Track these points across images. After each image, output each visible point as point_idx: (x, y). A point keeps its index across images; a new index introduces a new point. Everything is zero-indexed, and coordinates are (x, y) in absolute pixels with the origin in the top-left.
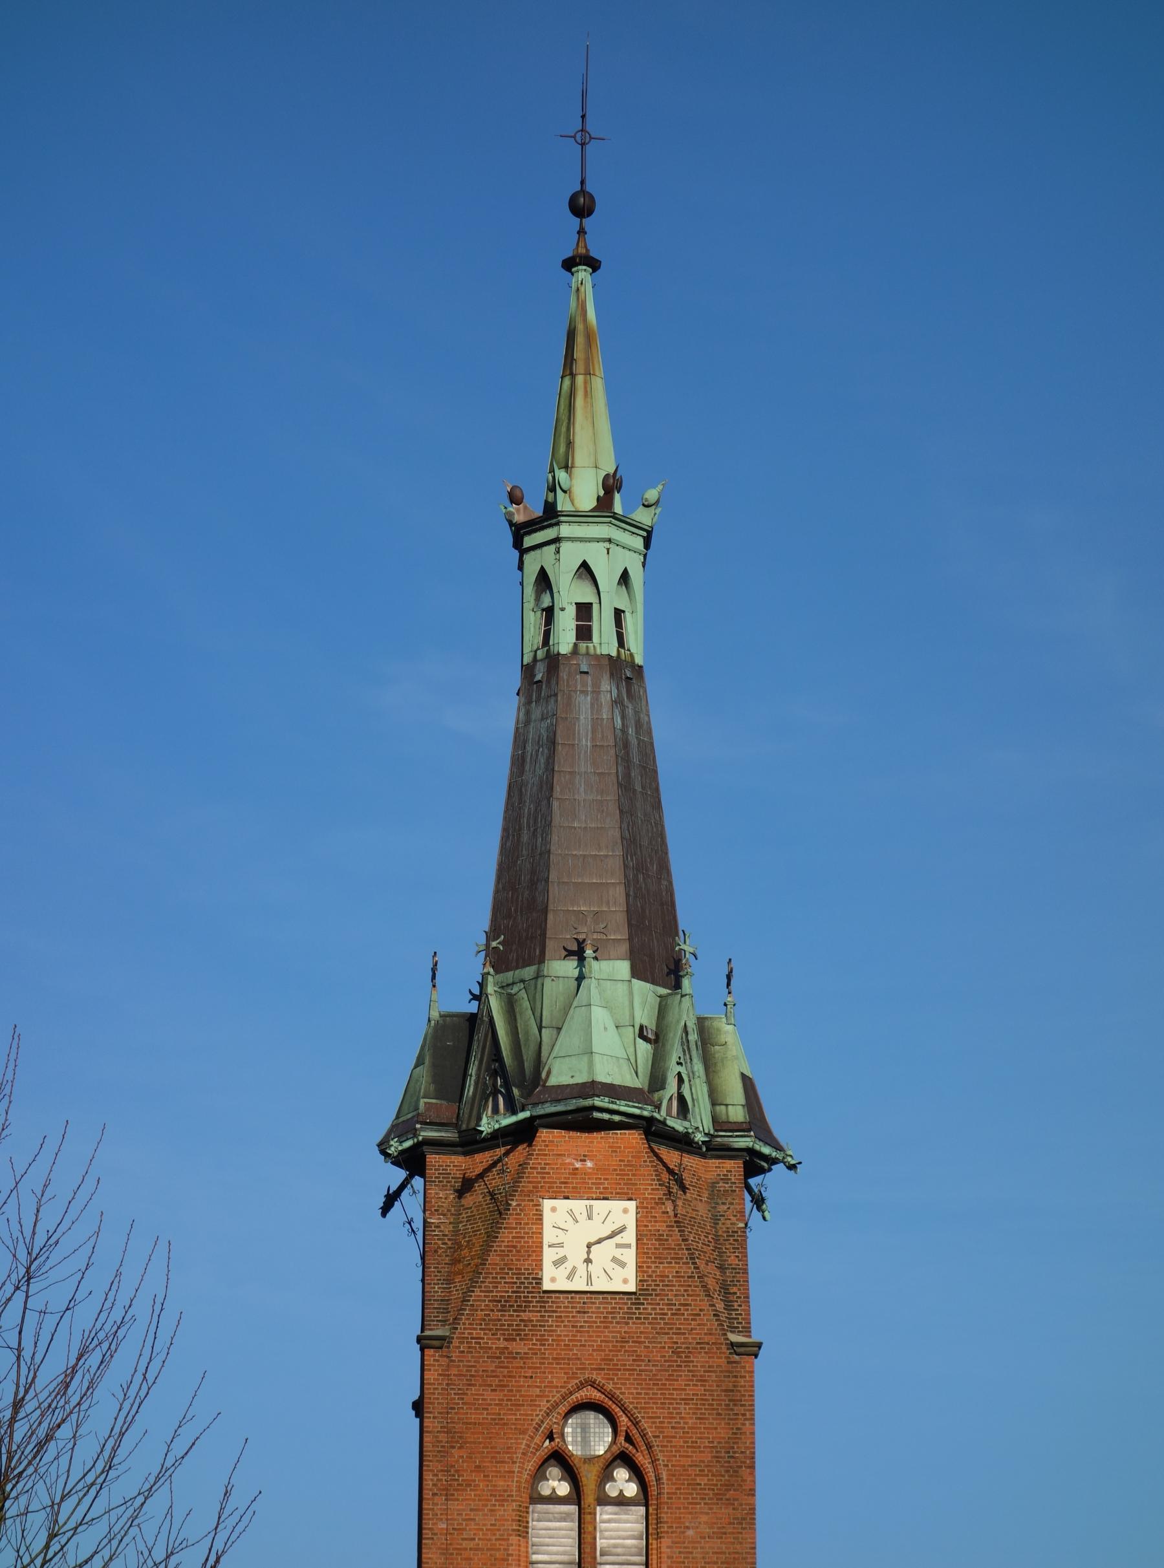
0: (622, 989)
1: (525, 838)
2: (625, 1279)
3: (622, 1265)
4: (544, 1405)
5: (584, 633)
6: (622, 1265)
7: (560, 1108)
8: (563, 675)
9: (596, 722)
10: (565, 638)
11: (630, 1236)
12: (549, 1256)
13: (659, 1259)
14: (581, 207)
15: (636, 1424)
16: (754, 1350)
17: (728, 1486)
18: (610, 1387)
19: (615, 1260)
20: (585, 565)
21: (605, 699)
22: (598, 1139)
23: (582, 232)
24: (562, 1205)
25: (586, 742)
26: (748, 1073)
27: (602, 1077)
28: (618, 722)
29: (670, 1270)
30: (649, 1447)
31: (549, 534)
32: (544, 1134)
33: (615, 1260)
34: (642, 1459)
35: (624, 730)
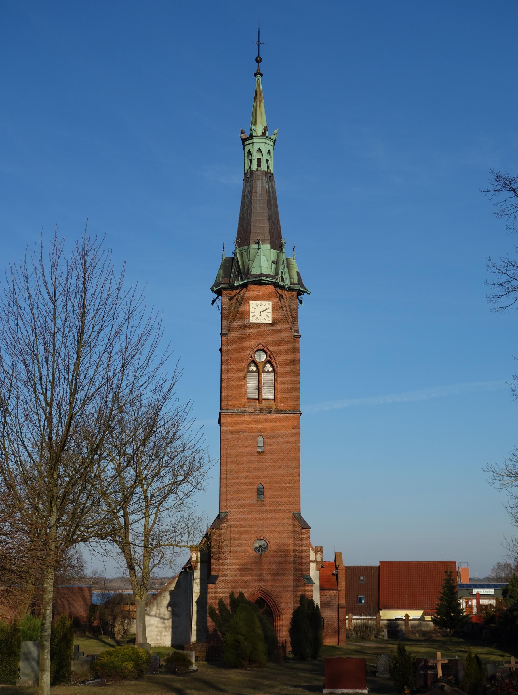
2: (269, 320)
3: (269, 317)
4: (250, 350)
5: (259, 165)
6: (269, 317)
9: (262, 187)
10: (255, 167)
11: (270, 310)
12: (251, 315)
13: (277, 315)
14: (258, 60)
17: (293, 368)
18: (265, 345)
19: (267, 315)
20: (259, 149)
21: (264, 181)
23: (258, 67)
25: (260, 192)
27: (264, 272)
30: (275, 359)
31: (251, 141)
32: (250, 286)
33: (267, 315)
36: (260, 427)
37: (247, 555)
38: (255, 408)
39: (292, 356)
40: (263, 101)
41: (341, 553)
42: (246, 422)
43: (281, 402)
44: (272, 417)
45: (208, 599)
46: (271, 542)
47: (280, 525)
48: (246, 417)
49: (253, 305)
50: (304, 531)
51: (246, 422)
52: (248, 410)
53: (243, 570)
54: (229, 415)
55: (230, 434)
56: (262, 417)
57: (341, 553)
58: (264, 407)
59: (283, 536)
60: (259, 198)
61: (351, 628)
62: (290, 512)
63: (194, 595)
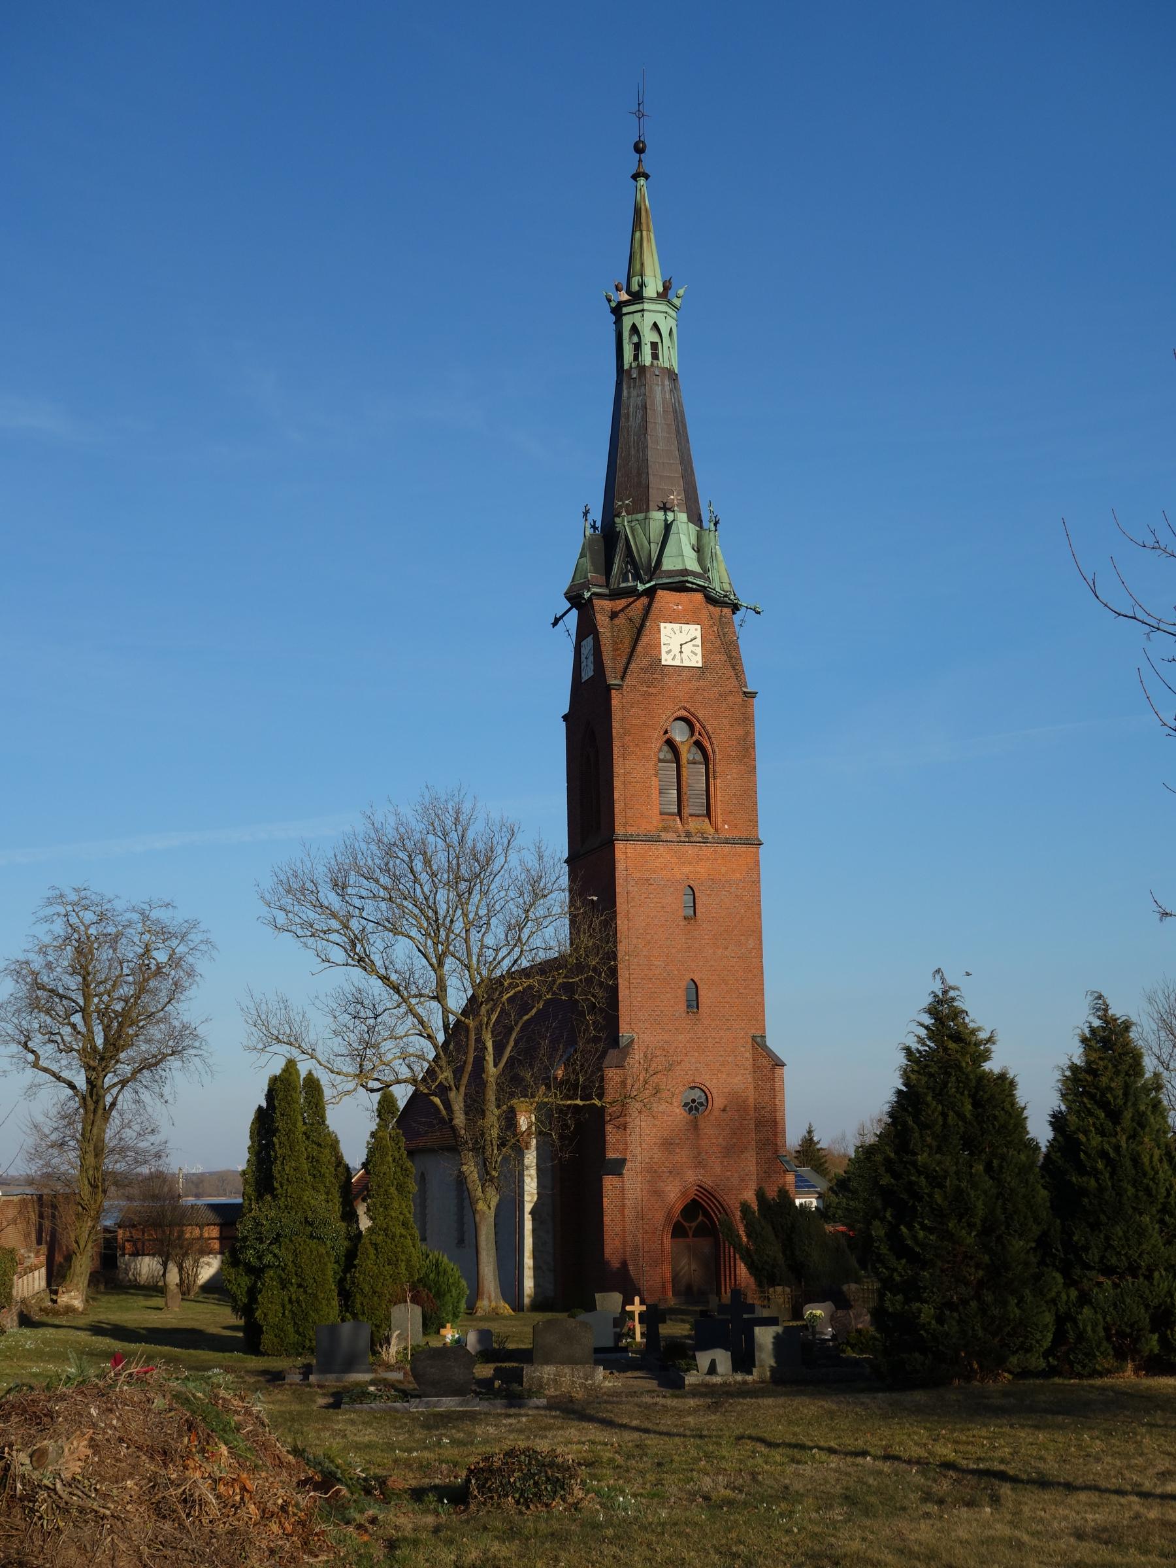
1: (633, 452)
2: (696, 661)
8: (648, 376)
9: (664, 399)
10: (647, 359)
11: (698, 641)
12: (664, 649)
13: (712, 652)
14: (639, 149)
15: (704, 727)
16: (753, 695)
17: (745, 757)
20: (655, 325)
21: (667, 388)
23: (640, 161)
25: (660, 409)
29: (717, 657)
30: (709, 738)
31: (638, 307)
32: (660, 592)
34: (706, 744)
36: (687, 869)
39: (741, 732)
40: (652, 229)
42: (661, 860)
43: (725, 822)
45: (605, 1204)
46: (714, 1091)
47: (730, 1059)
48: (661, 849)
50: (778, 1070)
51: (661, 860)
52: (664, 836)
53: (667, 1145)
54: (630, 845)
55: (633, 883)
56: (690, 850)
58: (693, 831)
60: (660, 420)
62: (747, 1033)
63: (527, 1198)
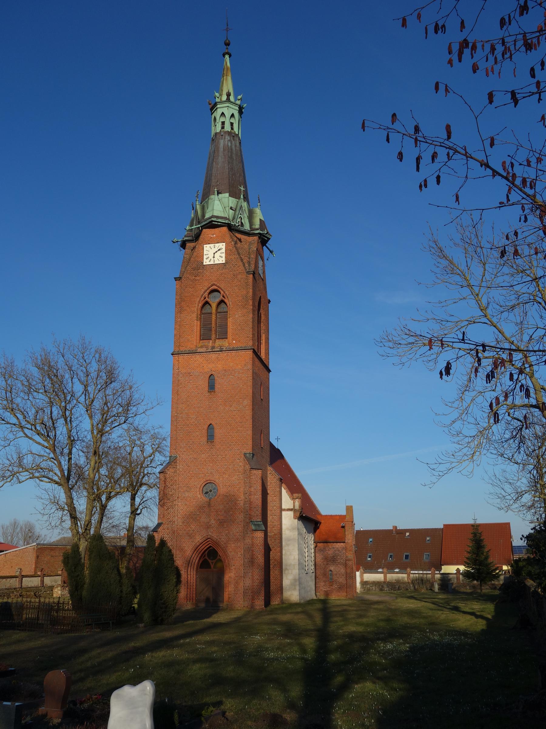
0: (227, 199)
3: (222, 257)
4: (203, 290)
5: (223, 128)
6: (222, 257)
7: (206, 223)
12: (205, 257)
13: (230, 255)
17: (246, 305)
18: (218, 285)
19: (220, 256)
22: (217, 230)
24: (208, 246)
26: (263, 219)
27: (215, 214)
28: (230, 144)
33: (220, 256)
35: (231, 146)
37: (195, 500)
38: (207, 347)
41: (352, 507)
43: (233, 339)
44: (223, 355)
49: (207, 247)
56: (213, 356)
57: (352, 507)
59: (233, 479)
61: (409, 581)
62: (241, 452)
